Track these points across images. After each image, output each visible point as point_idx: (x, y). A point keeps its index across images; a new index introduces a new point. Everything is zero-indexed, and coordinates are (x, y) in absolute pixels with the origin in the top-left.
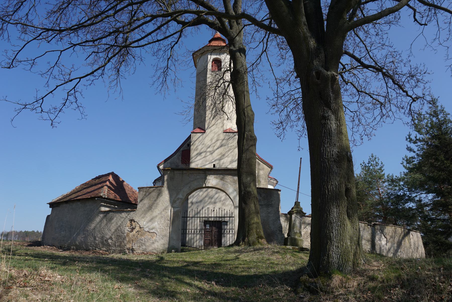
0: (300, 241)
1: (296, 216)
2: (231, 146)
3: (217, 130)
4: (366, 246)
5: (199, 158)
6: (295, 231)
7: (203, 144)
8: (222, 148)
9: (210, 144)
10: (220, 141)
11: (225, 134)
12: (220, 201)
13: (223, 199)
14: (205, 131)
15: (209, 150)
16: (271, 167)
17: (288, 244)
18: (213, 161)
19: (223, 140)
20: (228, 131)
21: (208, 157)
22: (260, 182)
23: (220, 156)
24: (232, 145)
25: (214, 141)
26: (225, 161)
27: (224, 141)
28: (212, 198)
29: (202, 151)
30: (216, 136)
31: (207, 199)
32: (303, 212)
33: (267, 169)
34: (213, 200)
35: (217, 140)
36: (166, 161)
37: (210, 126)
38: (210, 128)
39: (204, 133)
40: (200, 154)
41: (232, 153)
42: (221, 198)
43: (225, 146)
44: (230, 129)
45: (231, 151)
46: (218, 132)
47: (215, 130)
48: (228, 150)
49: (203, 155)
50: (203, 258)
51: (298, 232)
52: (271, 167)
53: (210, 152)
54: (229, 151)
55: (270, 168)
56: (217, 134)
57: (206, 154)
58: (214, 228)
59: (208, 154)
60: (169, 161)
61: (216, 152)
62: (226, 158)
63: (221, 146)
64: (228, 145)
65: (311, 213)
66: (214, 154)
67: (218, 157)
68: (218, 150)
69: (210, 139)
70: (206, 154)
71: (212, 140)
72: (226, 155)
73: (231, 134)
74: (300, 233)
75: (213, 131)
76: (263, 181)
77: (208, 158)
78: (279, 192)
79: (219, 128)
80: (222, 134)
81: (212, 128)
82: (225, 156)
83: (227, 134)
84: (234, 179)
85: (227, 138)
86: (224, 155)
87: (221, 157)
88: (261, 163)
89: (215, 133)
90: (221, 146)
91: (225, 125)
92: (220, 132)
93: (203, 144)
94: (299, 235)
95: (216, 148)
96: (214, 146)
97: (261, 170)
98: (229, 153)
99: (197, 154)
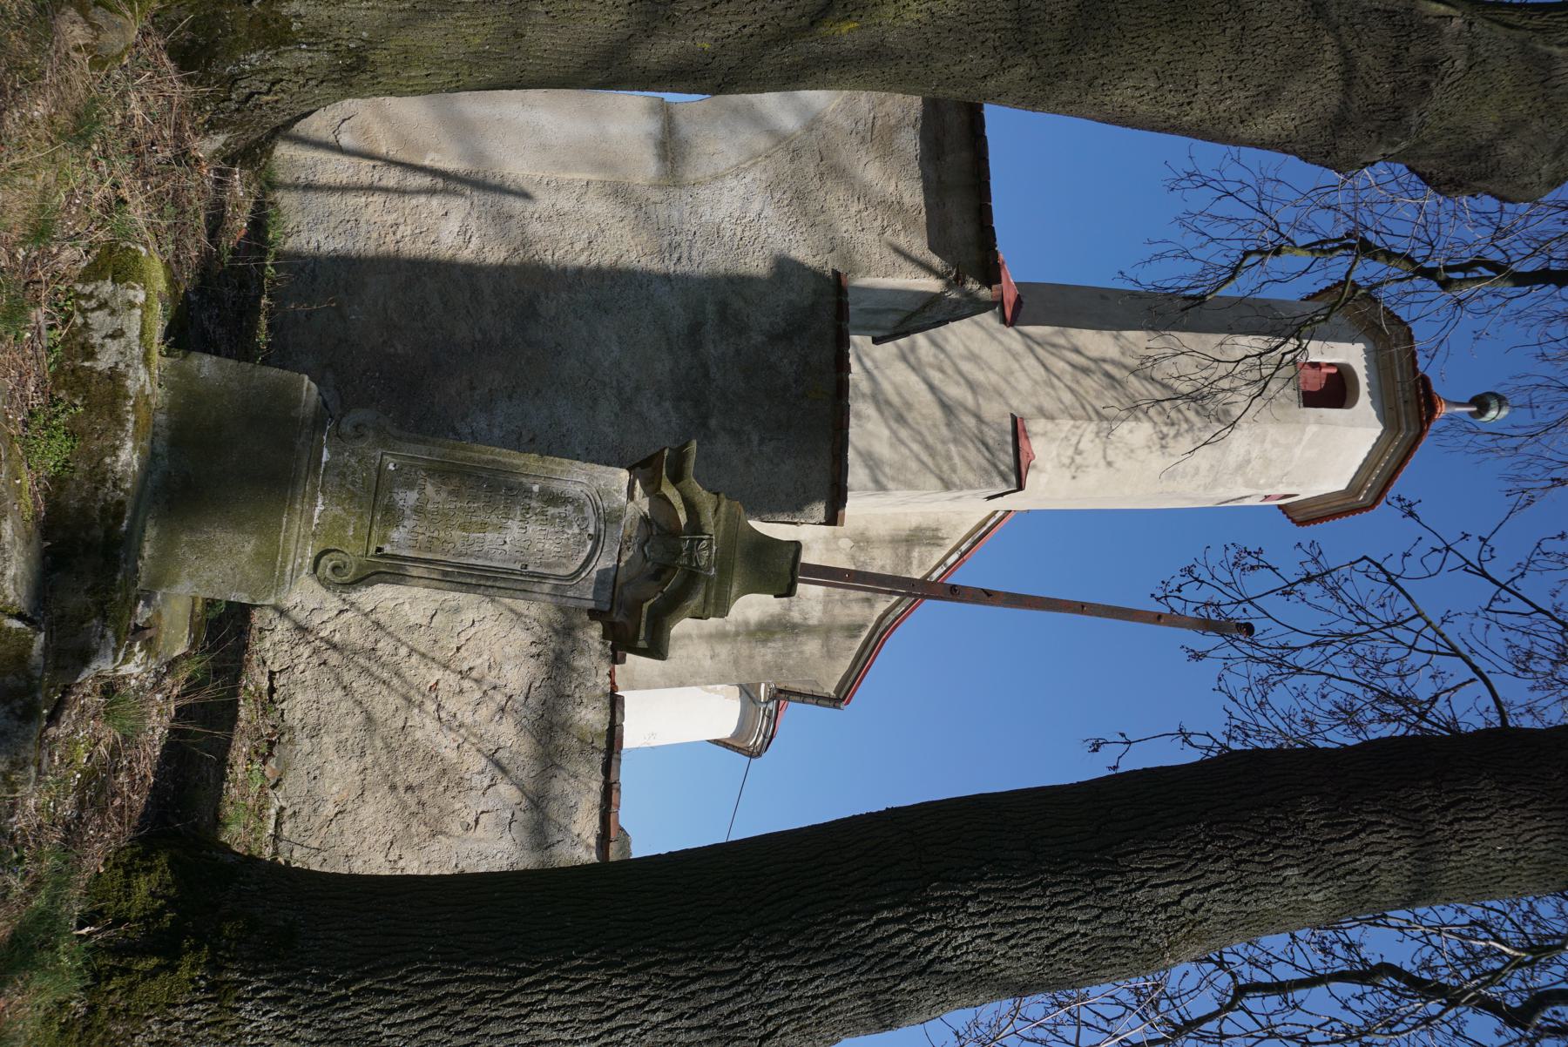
0: (250, 546)
1: (611, 518)
2: (949, 458)
3: (1025, 384)
6: (408, 498)
8: (938, 413)
9: (948, 348)
10: (969, 400)
11: (1008, 426)
14: (1012, 324)
17: (206, 366)
18: (869, 364)
19: (979, 418)
20: (1022, 442)
22: (765, 641)
23: (895, 400)
24: (957, 460)
25: (966, 367)
26: (870, 426)
27: (970, 422)
30: (994, 378)
32: (670, 608)
33: (830, 680)
35: (972, 386)
37: (1038, 350)
38: (1032, 351)
39: (1004, 321)
41: (914, 465)
43: (949, 425)
44: (1031, 456)
45: (925, 457)
46: (1014, 388)
47: (1020, 375)
48: (930, 440)
51: (399, 539)
54: (927, 447)
55: (839, 689)
56: (1003, 385)
61: (914, 379)
62: (886, 433)
63: (947, 407)
64: (956, 441)
65: (637, 852)
66: (901, 366)
67: (887, 387)
68: (923, 387)
69: (975, 347)
71: (973, 357)
72: (904, 433)
73: (1010, 460)
74: (389, 570)
75: (1016, 366)
76: (769, 657)
78: (819, 510)
79: (1035, 394)
80: (1008, 411)
81: (1030, 361)
82: (895, 426)
83: (1010, 439)
84: (897, 128)
85: (991, 436)
86: (901, 419)
87: (888, 403)
88: (857, 644)
89: (1006, 376)
90: (947, 407)
91: (1050, 426)
92: (1015, 402)
94: (354, 554)
95: (936, 377)
96: (942, 371)
97: (826, 644)
98: (915, 447)
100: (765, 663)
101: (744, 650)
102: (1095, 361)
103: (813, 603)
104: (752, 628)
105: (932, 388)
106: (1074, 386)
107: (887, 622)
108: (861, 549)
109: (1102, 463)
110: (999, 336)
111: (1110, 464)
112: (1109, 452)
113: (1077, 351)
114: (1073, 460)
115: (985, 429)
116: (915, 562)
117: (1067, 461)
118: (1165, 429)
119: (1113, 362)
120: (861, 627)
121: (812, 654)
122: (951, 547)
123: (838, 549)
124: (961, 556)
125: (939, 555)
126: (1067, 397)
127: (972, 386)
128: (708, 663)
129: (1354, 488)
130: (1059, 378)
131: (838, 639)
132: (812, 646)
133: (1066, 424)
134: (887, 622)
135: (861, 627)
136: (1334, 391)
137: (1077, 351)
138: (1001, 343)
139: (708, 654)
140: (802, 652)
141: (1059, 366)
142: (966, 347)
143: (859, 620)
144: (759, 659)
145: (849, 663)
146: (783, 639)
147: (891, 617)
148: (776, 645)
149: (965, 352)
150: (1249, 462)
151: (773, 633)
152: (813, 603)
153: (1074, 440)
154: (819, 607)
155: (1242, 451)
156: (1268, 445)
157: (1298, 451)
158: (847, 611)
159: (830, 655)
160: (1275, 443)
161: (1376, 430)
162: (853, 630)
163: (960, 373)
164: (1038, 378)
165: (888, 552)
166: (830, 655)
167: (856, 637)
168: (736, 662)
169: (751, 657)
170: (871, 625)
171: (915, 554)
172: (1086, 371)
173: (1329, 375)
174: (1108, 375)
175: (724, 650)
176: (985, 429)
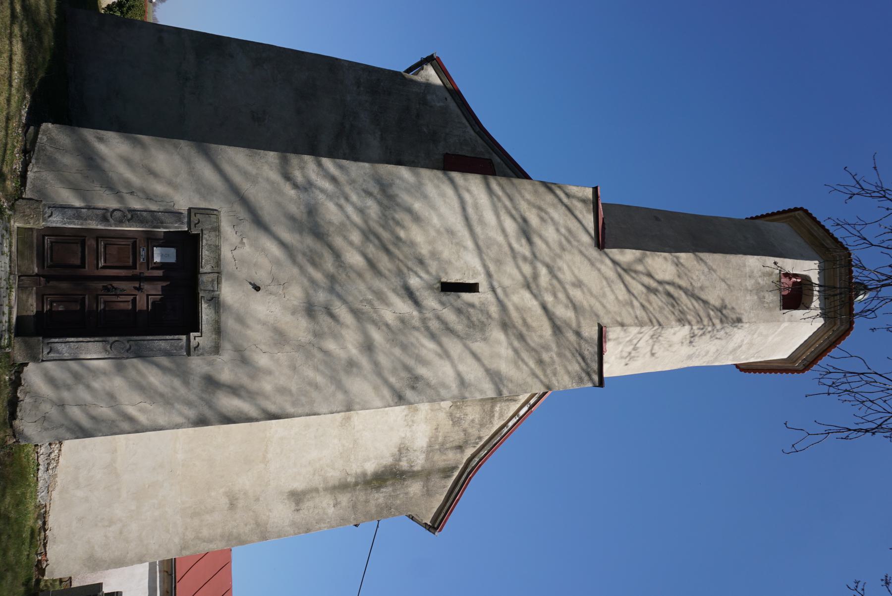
4: (24, 558)
5: (510, 226)
7: (563, 249)
12: (318, 335)
13: (331, 345)
15: (543, 271)
16: (435, 526)
19: (578, 334)
21: (515, 272)
22: (378, 488)
23: (518, 322)
24: (560, 369)
25: (576, 294)
27: (572, 337)
28: (332, 290)
29: (536, 240)
31: (329, 264)
34: (321, 297)
35: (575, 307)
36: (456, 94)
37: (627, 278)
40: (526, 232)
42: (336, 337)
49: (523, 248)
50: (9, 288)
52: (435, 526)
53: (536, 276)
55: (434, 519)
57: (525, 259)
58: (154, 291)
59: (527, 269)
60: (452, 105)
61: (533, 304)
63: (557, 329)
68: (539, 311)
70: (525, 259)
71: (579, 284)
76: (381, 500)
77: (510, 268)
88: (450, 482)
93: (563, 249)
95: (549, 299)
99: (525, 220)
100: (377, 506)
101: (361, 496)
102: (660, 283)
103: (418, 453)
104: (368, 478)
105: (544, 308)
106: (646, 304)
107: (473, 463)
108: (458, 407)
109: (649, 354)
110: (598, 265)
111: (653, 354)
112: (656, 347)
113: (650, 275)
114: (630, 353)
115: (583, 344)
116: (497, 415)
117: (625, 354)
118: (696, 332)
119: (671, 283)
120: (454, 468)
121: (415, 494)
122: (523, 401)
123: (440, 409)
124: (530, 408)
125: (514, 407)
126: (640, 312)
127: (575, 307)
128: (331, 510)
129: (792, 358)
130: (636, 298)
131: (436, 480)
132: (415, 488)
133: (634, 330)
134: (473, 463)
135: (454, 468)
136: (794, 297)
137: (650, 275)
138: (599, 270)
139: (332, 503)
140: (407, 494)
141: (637, 288)
142: (575, 276)
143: (452, 463)
144: (373, 502)
145: (442, 498)
146: (393, 484)
147: (477, 459)
148: (387, 490)
149: (574, 279)
150: (740, 346)
151: (385, 481)
152: (418, 453)
153: (635, 341)
154: (422, 457)
155: (739, 341)
156: (755, 336)
157: (770, 339)
158: (444, 457)
159: (428, 493)
160: (761, 334)
161: (820, 322)
162: (446, 472)
163: (568, 297)
164: (621, 298)
165: (478, 408)
166: (428, 493)
167: (450, 476)
168: (354, 507)
169: (367, 501)
170: (461, 467)
171: (497, 409)
172: (654, 291)
173: (794, 283)
174: (669, 295)
175: (344, 499)
176: (583, 344)
